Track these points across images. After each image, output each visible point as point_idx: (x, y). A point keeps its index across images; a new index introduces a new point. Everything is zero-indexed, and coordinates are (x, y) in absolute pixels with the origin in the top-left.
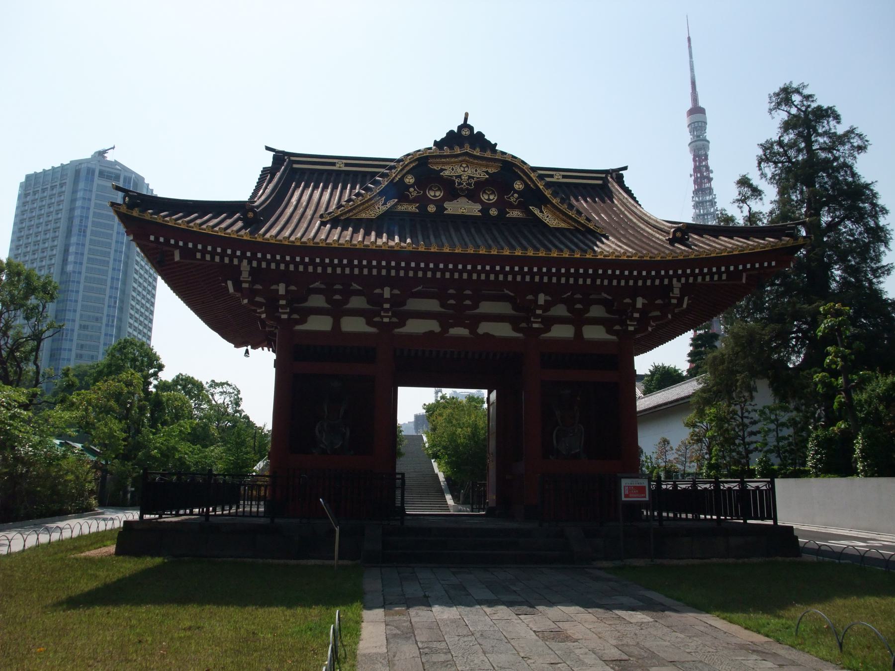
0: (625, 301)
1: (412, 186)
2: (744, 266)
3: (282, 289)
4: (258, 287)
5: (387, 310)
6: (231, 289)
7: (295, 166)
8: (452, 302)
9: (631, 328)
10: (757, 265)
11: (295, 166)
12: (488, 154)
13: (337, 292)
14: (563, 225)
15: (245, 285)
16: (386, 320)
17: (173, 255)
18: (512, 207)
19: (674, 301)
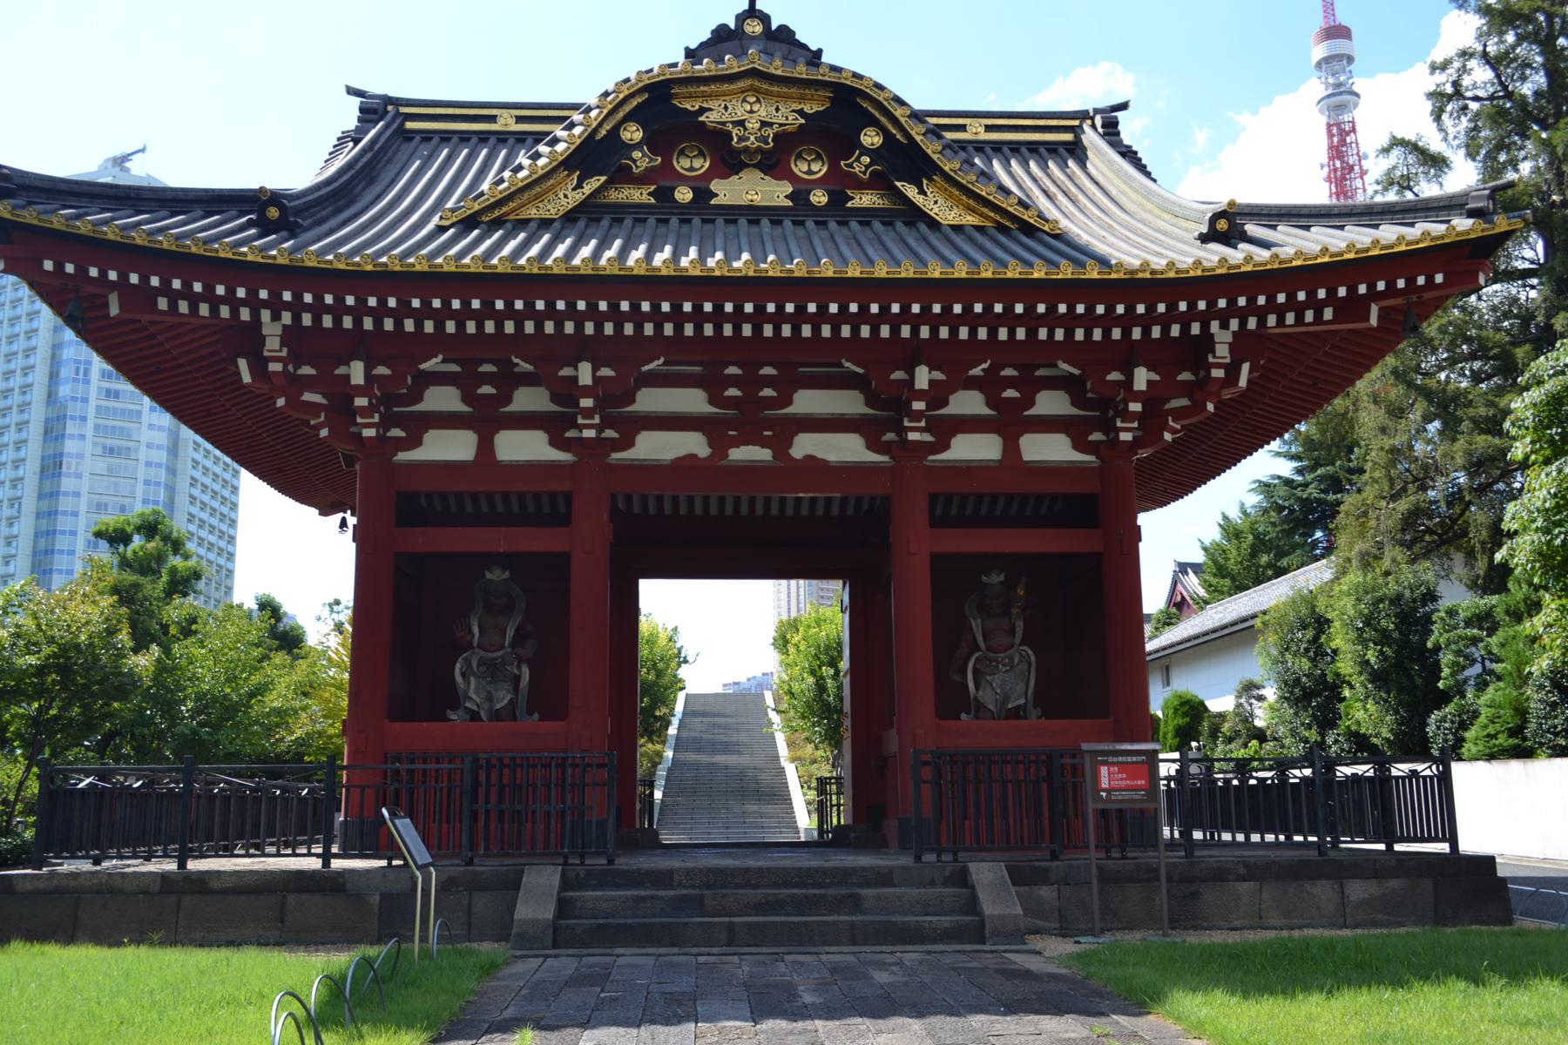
0: (1110, 377)
1: (638, 146)
2: (1371, 286)
3: (357, 372)
4: (307, 370)
5: (588, 413)
6: (246, 378)
7: (409, 125)
8: (733, 392)
9: (1126, 437)
10: (1401, 283)
11: (409, 125)
12: (801, 71)
13: (487, 378)
14: (970, 219)
15: (275, 367)
16: (589, 433)
17: (106, 305)
18: (861, 186)
19: (1218, 373)
